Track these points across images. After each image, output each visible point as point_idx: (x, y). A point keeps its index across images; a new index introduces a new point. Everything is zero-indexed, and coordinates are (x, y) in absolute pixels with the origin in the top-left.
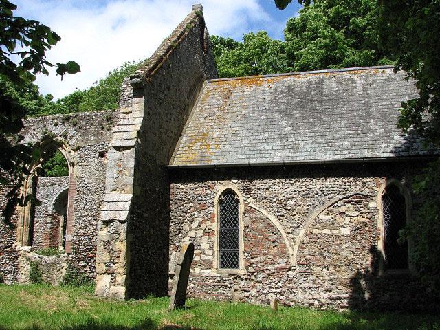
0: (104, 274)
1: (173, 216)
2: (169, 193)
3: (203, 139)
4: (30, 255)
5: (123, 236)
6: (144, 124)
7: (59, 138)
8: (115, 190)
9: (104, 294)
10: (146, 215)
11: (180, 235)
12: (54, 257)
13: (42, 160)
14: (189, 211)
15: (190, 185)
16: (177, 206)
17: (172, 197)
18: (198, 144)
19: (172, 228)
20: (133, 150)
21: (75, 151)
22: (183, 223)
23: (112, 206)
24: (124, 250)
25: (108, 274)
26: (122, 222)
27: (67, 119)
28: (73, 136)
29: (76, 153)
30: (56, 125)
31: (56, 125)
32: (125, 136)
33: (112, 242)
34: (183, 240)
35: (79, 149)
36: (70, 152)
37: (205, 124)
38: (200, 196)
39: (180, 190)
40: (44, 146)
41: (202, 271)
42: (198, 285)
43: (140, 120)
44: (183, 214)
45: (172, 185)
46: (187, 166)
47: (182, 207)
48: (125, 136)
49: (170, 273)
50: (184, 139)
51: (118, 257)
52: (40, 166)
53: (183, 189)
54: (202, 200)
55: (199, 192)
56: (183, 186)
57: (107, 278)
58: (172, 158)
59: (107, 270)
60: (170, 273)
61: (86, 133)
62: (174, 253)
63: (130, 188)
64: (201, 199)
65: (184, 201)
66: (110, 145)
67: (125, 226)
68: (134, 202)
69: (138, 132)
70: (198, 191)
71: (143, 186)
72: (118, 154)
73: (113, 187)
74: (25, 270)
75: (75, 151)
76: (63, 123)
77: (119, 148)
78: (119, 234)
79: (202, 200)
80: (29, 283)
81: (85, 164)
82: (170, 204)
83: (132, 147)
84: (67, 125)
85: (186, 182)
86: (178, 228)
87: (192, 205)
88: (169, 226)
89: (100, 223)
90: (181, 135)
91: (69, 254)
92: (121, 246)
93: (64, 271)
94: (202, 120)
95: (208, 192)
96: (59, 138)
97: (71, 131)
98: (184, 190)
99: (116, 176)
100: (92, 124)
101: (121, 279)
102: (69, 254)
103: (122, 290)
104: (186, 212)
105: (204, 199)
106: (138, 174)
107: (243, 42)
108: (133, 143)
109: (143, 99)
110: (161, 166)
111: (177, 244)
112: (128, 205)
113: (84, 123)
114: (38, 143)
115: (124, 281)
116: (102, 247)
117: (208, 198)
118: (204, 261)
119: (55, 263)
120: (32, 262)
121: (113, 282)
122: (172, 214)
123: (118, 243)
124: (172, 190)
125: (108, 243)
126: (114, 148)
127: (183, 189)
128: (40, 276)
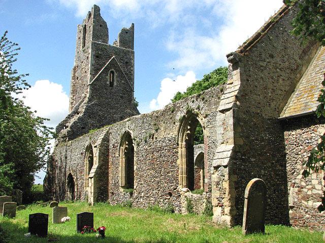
0: (217, 206)
1: (288, 158)
2: (283, 139)
3: (310, 91)
4: (186, 194)
5: (227, 177)
6: (240, 90)
7: (196, 110)
8: (223, 143)
9: (218, 221)
10: (253, 160)
11: (295, 173)
12: (199, 195)
13: (189, 127)
14: (299, 153)
15: (299, 131)
16: (290, 149)
17: (286, 143)
18: (306, 96)
19: (288, 168)
20: (232, 110)
21: (205, 118)
22: (296, 163)
23: (220, 155)
24: (228, 188)
25: (220, 206)
26: (225, 167)
27: (69, 118)
28: (202, 108)
29: (206, 119)
30: (193, 102)
31: (193, 102)
32: (228, 101)
33: (220, 182)
34: (297, 177)
35: (206, 116)
36: (202, 119)
37: (315, 78)
38: (307, 139)
39: (291, 136)
40: (189, 117)
41: (314, 203)
42: (312, 216)
43: (238, 88)
44: (296, 156)
45: (285, 133)
46: (293, 116)
47: (294, 150)
48: (228, 101)
49: (290, 205)
50: (296, 93)
51: (225, 193)
52: (189, 132)
53: (294, 135)
54: (308, 143)
55: (306, 136)
56: (293, 133)
57: (219, 209)
58: (284, 111)
59: (219, 203)
60: (290, 205)
61: (210, 105)
62: (292, 188)
63: (231, 141)
64: (307, 141)
65: (296, 145)
66: (218, 110)
67: (227, 170)
68: (235, 151)
69: (236, 96)
70: (305, 136)
71: (247, 137)
72: (223, 115)
73: (222, 141)
74: (185, 204)
75: (205, 118)
76: (197, 99)
77: (223, 111)
78: (224, 176)
79: (308, 143)
80: (187, 213)
81: (211, 126)
82: (285, 149)
83: (231, 108)
84: (199, 100)
85: (295, 129)
86: (293, 167)
87: (301, 147)
88: (286, 167)
89: (212, 168)
90: (293, 91)
91: (207, 192)
92: (226, 185)
93: (204, 204)
94: (313, 75)
95: (313, 135)
96: (196, 110)
97: (202, 104)
98: (295, 136)
99: (223, 132)
100: (213, 97)
101: (227, 210)
102: (207, 192)
103: (228, 218)
104: (298, 154)
105: (310, 141)
106: (239, 129)
107: (11, 92)
108: (230, 106)
109: (238, 70)
110: (269, 119)
111: (293, 181)
112: (229, 154)
113: (208, 96)
114: (184, 116)
115: (229, 212)
116: (215, 186)
117: (313, 140)
118: (315, 194)
119: (200, 199)
120: (187, 199)
121: (223, 213)
122: (287, 156)
123: (224, 183)
124: (285, 137)
125: (218, 184)
126: (220, 111)
127: (294, 135)
128: (192, 209)
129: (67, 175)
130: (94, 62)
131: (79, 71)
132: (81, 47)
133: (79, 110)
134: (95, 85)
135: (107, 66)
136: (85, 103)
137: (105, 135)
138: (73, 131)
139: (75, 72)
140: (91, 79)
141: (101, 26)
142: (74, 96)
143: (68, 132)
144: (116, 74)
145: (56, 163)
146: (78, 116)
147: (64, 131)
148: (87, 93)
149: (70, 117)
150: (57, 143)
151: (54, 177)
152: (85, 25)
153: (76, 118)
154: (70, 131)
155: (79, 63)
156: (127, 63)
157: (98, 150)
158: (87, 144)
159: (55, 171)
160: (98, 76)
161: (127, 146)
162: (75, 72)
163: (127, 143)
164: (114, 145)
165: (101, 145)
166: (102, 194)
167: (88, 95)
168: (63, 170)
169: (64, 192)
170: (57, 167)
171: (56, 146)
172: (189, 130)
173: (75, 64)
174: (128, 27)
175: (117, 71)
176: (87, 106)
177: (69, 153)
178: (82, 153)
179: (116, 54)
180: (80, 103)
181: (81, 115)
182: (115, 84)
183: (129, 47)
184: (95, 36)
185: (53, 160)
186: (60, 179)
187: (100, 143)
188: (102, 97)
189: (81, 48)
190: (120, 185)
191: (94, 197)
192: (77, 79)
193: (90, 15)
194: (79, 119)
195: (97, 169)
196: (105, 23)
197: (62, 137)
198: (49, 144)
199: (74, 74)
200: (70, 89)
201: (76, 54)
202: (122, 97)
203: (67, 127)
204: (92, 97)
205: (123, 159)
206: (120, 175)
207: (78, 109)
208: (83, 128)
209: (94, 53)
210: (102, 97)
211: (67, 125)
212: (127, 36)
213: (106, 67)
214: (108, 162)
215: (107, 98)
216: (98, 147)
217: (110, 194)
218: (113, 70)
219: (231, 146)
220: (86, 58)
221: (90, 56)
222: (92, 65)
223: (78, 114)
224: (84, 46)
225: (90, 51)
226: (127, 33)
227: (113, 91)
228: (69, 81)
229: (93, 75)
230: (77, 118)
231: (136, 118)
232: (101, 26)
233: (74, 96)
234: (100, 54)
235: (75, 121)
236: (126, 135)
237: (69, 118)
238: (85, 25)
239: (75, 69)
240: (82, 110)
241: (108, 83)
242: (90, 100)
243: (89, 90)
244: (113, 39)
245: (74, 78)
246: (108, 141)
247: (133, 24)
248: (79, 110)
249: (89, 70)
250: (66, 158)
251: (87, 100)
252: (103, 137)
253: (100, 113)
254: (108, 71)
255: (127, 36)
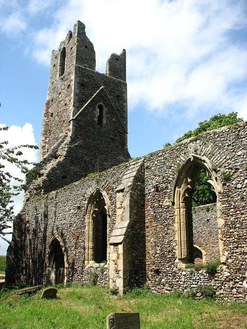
27: (44, 163)
112: (124, 230)
129: (50, 240)
130: (78, 91)
131: (55, 105)
132: (58, 75)
133: (59, 153)
134: (80, 120)
135: (94, 97)
136: (66, 144)
137: (138, 170)
138: (50, 180)
139: (48, 108)
140: (74, 114)
141: (86, 47)
142: (46, 138)
143: (44, 182)
144: (105, 109)
145: (28, 225)
146: (57, 160)
147: (39, 181)
148: (68, 131)
149: (45, 161)
150: (28, 196)
151: (23, 248)
152: (64, 48)
153: (53, 163)
154: (46, 181)
155: (55, 96)
156: (118, 96)
157: (128, 195)
158: (91, 191)
159: (26, 237)
160: (83, 110)
161: (189, 186)
162: (48, 108)
163: (189, 180)
164: (157, 189)
165: (134, 188)
166: (136, 273)
167: (70, 134)
168: (41, 235)
169: (42, 267)
170: (28, 231)
171: (27, 201)
172: (188, 184)
173: (48, 98)
174: (119, 53)
175: (107, 105)
176: (69, 148)
177: (51, 209)
178: (79, 208)
179: (105, 84)
180: (59, 145)
181: (61, 159)
182: (105, 121)
183: (121, 78)
184: (79, 59)
185: (22, 220)
186: (36, 248)
187: (130, 184)
188: (88, 137)
189: (58, 77)
190: (178, 255)
191: (124, 279)
192: (52, 116)
193: (71, 35)
194: (59, 164)
195: (128, 227)
196: (91, 45)
197: (35, 189)
198: (11, 202)
199: (47, 110)
200: (42, 129)
201: (49, 85)
202: (113, 139)
203: (42, 175)
204: (76, 136)
205: (182, 210)
206: (177, 238)
207: (57, 151)
208: (64, 177)
209: (78, 80)
210: (88, 137)
211: (42, 172)
212: (118, 63)
213: (93, 99)
214: (144, 217)
215: (94, 140)
216: (127, 190)
217: (150, 274)
218: (101, 103)
219: (128, 221)
220: (66, 87)
221: (73, 83)
222: (76, 95)
223: (56, 158)
224: (62, 71)
225: (73, 77)
226: (117, 60)
227: (103, 130)
228: (42, 118)
229: (77, 107)
230: (56, 162)
231: (215, 133)
232: (86, 47)
233: (46, 138)
234: (87, 80)
235: (53, 167)
236: (189, 165)
237: (44, 163)
238: (64, 48)
239: (48, 104)
240: (62, 152)
241: (96, 119)
242: (73, 140)
243: (71, 127)
244: (101, 66)
245: (46, 115)
246: (143, 182)
247: (124, 50)
248: (59, 153)
249: (72, 101)
250: (46, 216)
251: (68, 139)
252: (134, 174)
253: (87, 158)
254: (96, 104)
255: (118, 63)
